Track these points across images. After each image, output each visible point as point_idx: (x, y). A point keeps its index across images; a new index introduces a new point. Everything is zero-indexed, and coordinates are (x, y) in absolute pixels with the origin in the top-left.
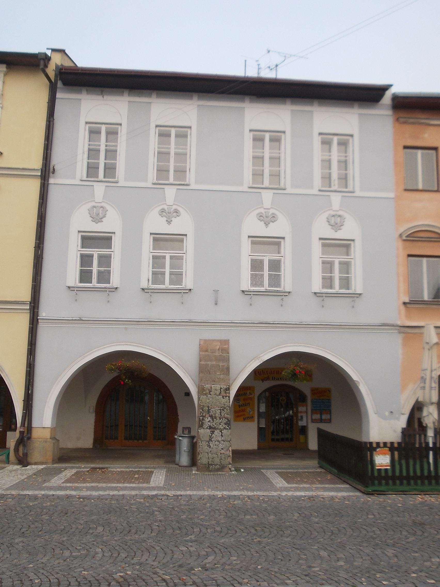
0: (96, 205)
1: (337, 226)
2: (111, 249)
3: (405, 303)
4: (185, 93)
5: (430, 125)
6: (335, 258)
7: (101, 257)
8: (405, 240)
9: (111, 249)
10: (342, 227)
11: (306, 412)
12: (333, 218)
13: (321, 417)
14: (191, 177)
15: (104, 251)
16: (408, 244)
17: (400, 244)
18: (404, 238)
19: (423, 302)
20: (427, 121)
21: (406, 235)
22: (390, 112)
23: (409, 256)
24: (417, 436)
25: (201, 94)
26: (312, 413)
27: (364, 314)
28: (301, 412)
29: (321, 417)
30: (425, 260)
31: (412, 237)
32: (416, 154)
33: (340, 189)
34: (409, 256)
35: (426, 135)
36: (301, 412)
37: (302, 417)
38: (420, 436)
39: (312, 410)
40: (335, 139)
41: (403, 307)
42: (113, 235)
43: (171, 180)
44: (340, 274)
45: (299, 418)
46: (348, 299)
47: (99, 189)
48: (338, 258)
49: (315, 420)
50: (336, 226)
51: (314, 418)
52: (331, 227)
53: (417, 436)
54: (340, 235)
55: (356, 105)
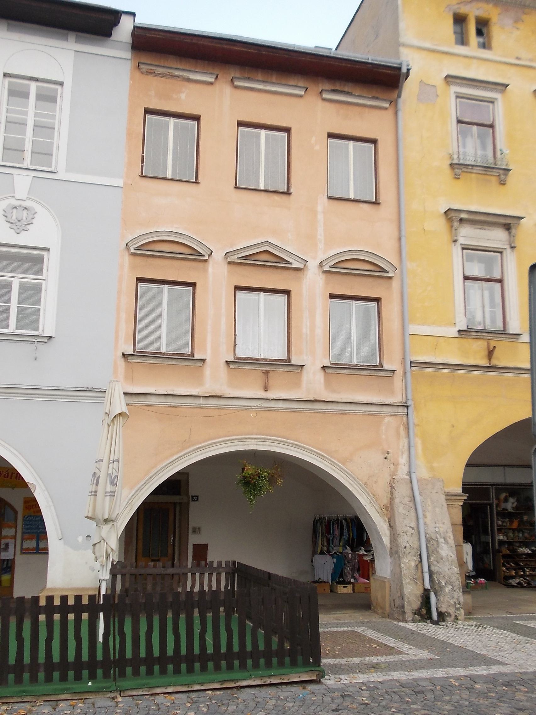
0: (17, 203)
1: (20, 226)
2: (42, 275)
3: (323, 368)
4: (41, 27)
5: (188, 80)
6: (14, 277)
7: (23, 287)
8: (133, 254)
9: (42, 275)
10: (28, 227)
11: (15, 537)
12: (15, 210)
13: (38, 544)
14: (60, 160)
15: (31, 279)
16: (138, 260)
17: (127, 258)
18: (133, 251)
19: (158, 355)
20: (185, 74)
21: (135, 246)
22: (127, 54)
23: (332, 296)
24: (189, 575)
25: (80, 34)
26: (23, 539)
27: (53, 369)
28: (6, 537)
29: (38, 544)
30: (166, 287)
31: (146, 250)
32: (258, 136)
33: (34, 167)
34: (332, 296)
35: (183, 96)
36: (6, 537)
37: (7, 545)
38: (193, 575)
39: (23, 533)
40: (33, 86)
41: (121, 362)
42: (45, 253)
43: (27, 163)
44: (18, 304)
45: (3, 546)
46: (27, 345)
47: (22, 182)
48: (19, 278)
49: (28, 549)
50: (19, 224)
51: (25, 546)
52: (10, 225)
53: (189, 575)
54: (23, 239)
55: (72, 37)
